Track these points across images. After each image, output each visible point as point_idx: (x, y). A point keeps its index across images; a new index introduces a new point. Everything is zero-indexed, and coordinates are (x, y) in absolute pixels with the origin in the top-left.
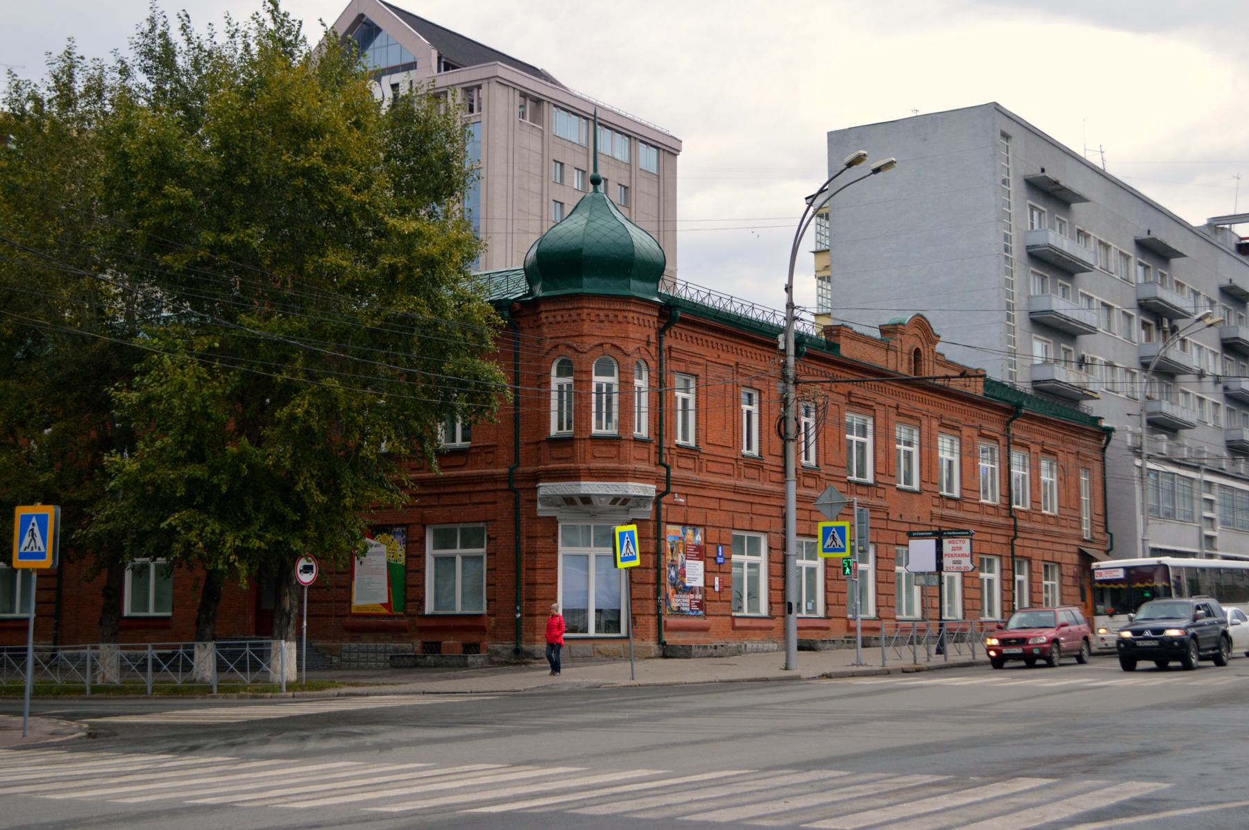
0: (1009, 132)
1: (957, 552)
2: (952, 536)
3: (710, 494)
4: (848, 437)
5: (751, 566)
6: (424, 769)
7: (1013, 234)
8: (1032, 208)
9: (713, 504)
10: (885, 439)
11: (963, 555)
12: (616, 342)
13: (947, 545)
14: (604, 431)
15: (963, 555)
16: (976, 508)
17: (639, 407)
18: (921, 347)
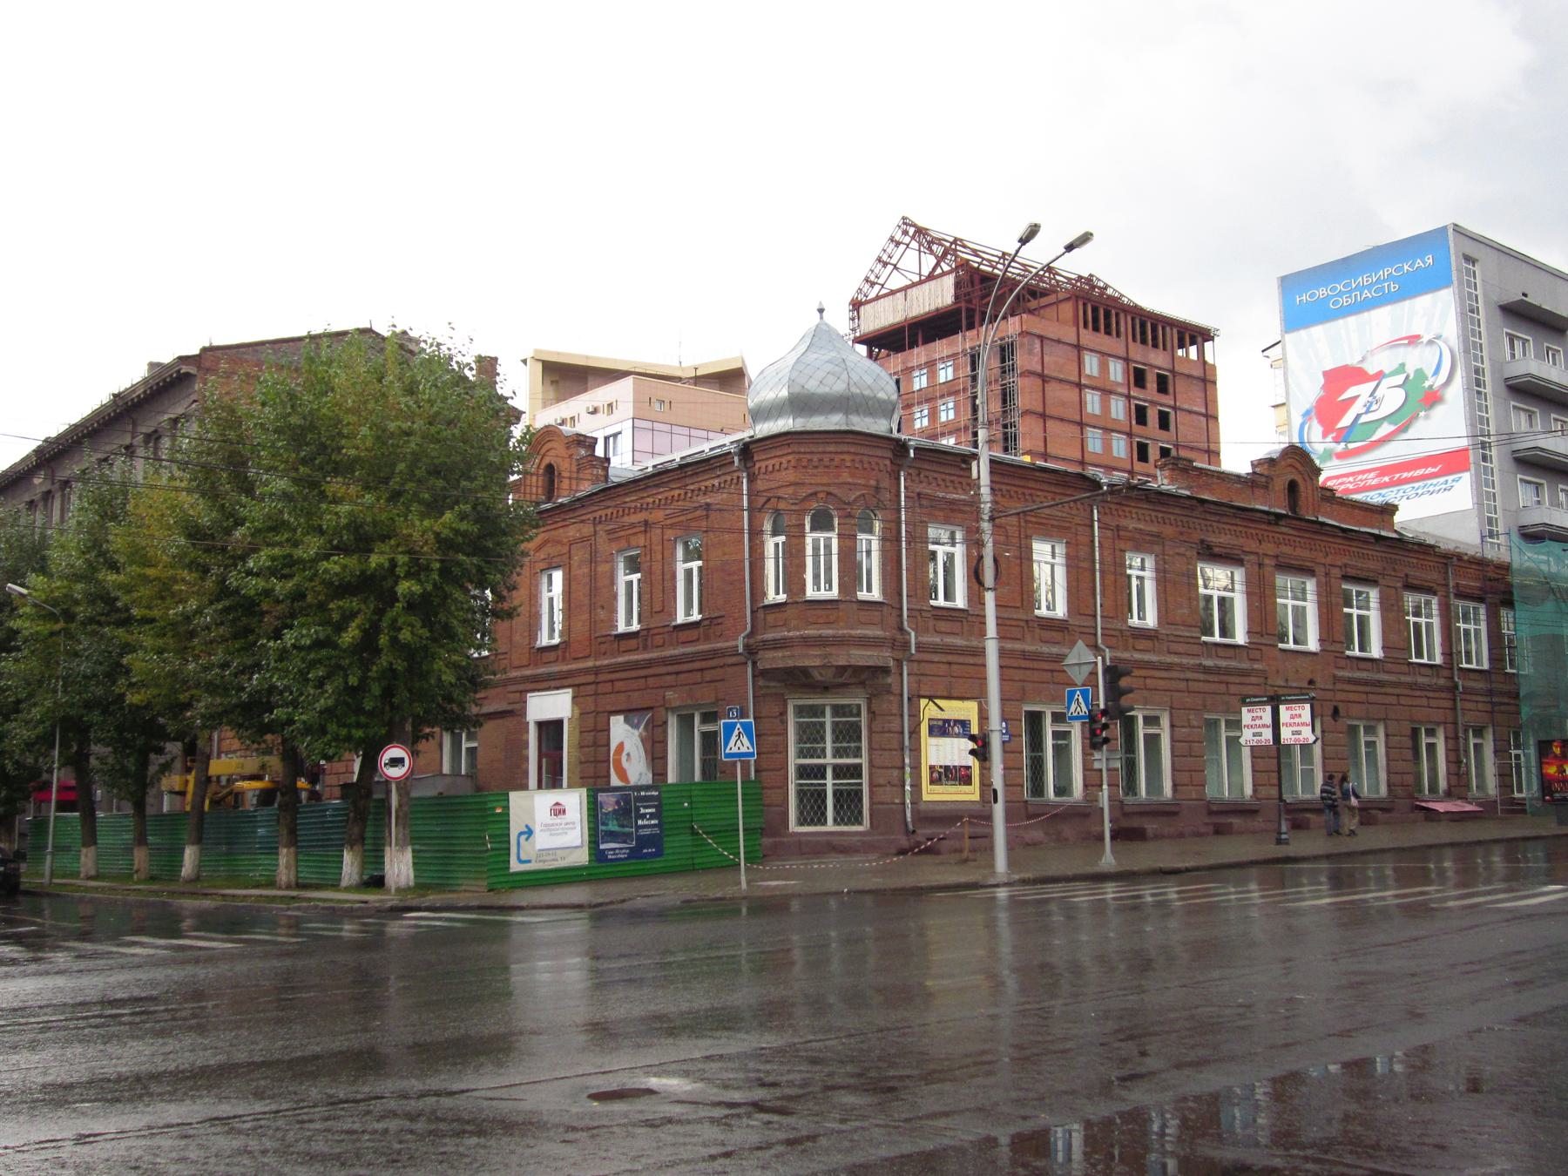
0: (1475, 255)
1: (1297, 720)
2: (1252, 704)
3: (1389, 690)
4: (1346, 610)
5: (824, 750)
6: (1498, 901)
7: (1486, 366)
8: (1512, 338)
9: (1393, 700)
10: (1392, 612)
11: (1303, 724)
12: (831, 489)
13: (1285, 713)
14: (823, 594)
15: (1303, 724)
16: (1405, 668)
17: (777, 558)
18: (1300, 481)
